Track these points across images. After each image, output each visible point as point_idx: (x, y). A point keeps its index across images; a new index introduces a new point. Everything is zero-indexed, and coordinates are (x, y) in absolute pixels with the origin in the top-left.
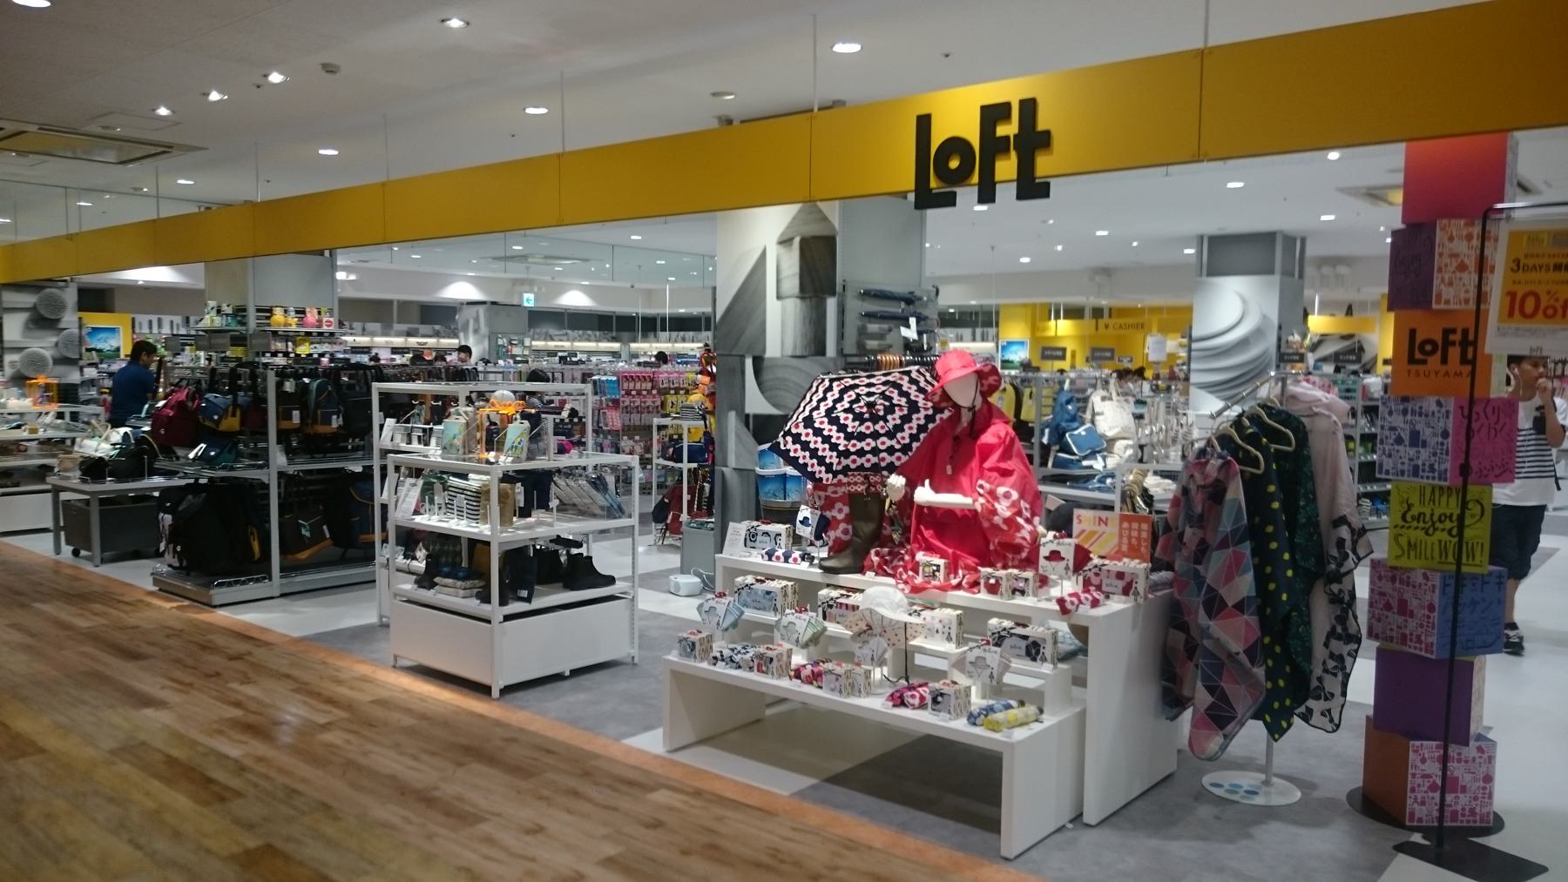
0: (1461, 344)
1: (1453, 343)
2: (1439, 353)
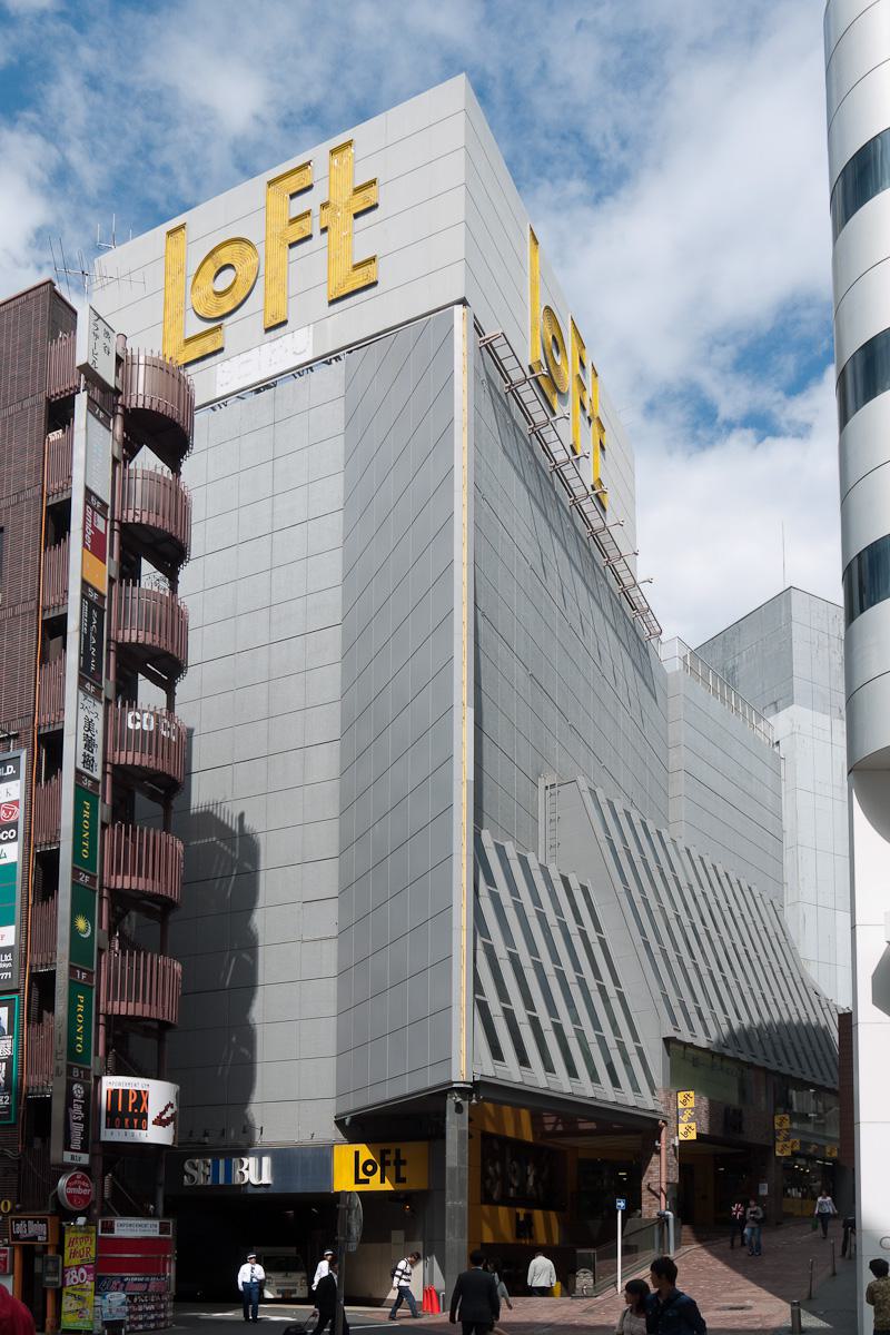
0: (395, 1164)
2: (362, 1161)
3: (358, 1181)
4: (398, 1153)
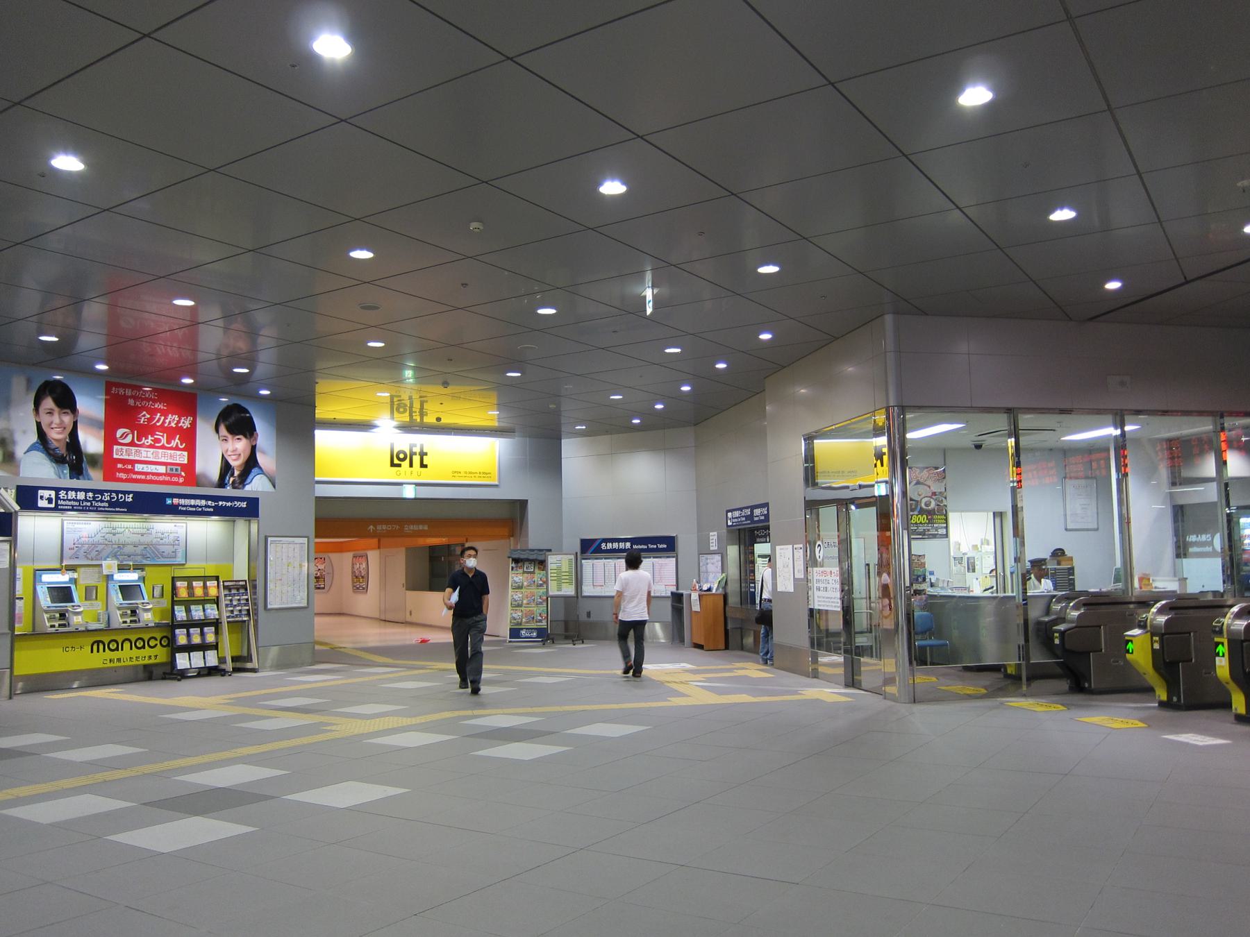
1: (415, 454)
3: (393, 465)
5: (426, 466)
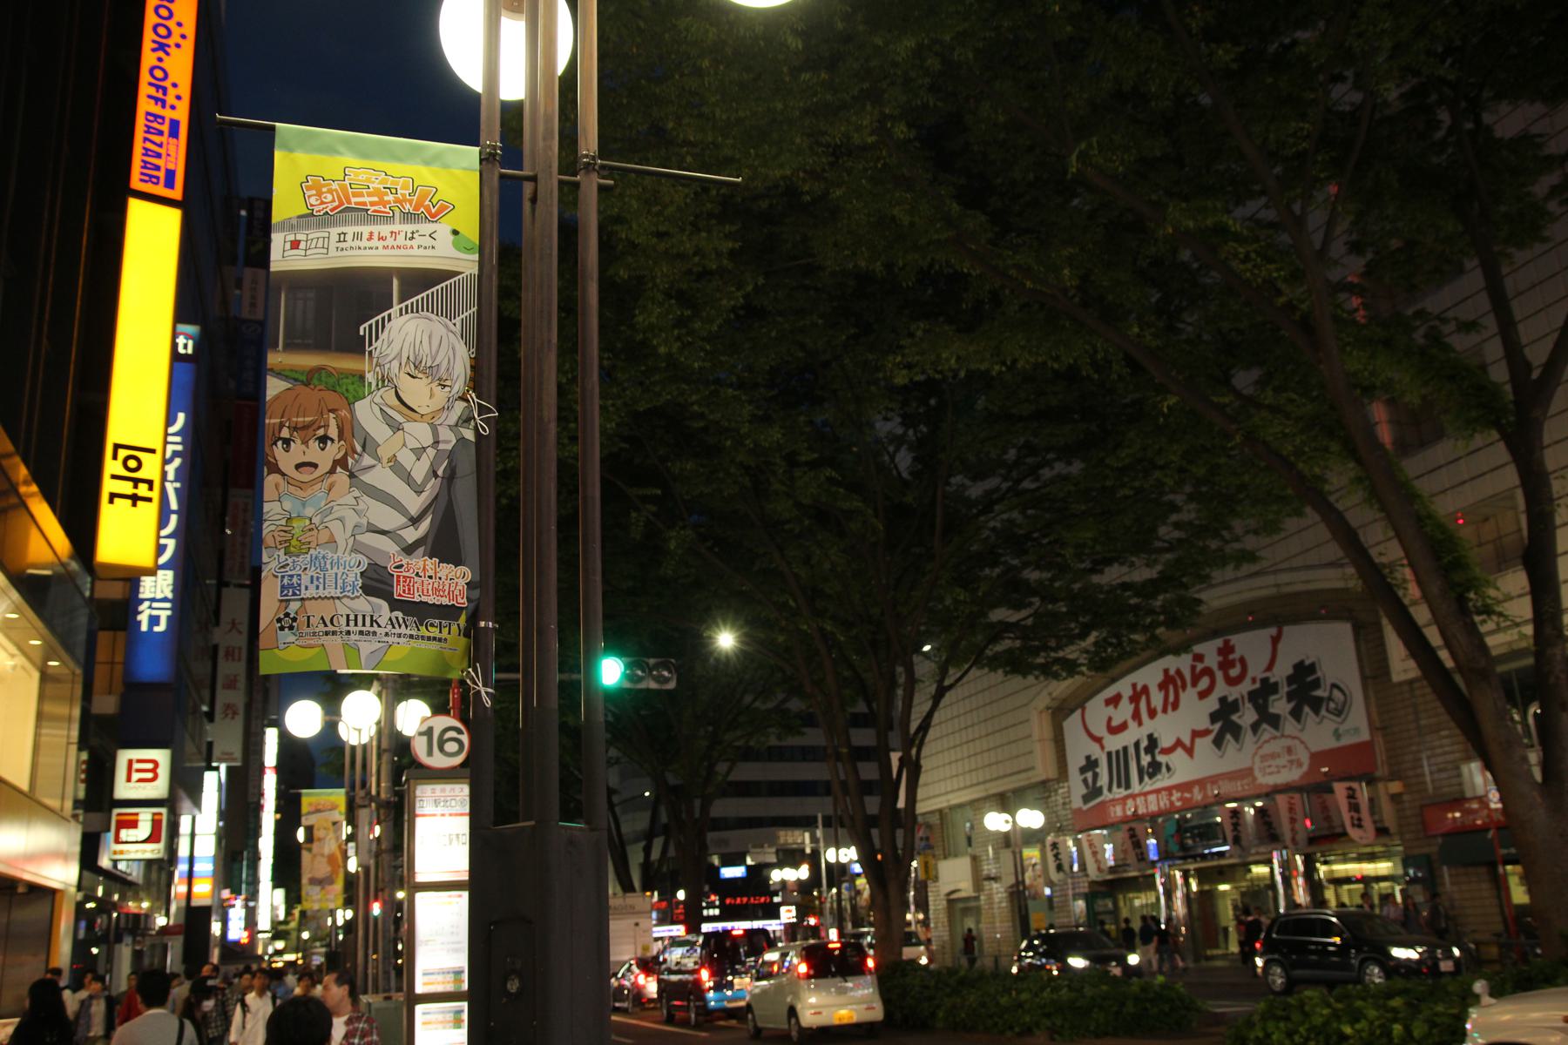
1: (136, 487)
3: (117, 447)
4: (149, 500)
5: (111, 502)
